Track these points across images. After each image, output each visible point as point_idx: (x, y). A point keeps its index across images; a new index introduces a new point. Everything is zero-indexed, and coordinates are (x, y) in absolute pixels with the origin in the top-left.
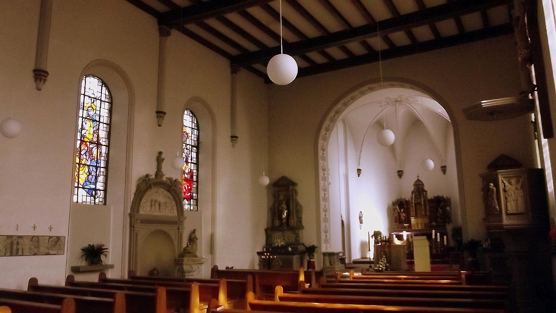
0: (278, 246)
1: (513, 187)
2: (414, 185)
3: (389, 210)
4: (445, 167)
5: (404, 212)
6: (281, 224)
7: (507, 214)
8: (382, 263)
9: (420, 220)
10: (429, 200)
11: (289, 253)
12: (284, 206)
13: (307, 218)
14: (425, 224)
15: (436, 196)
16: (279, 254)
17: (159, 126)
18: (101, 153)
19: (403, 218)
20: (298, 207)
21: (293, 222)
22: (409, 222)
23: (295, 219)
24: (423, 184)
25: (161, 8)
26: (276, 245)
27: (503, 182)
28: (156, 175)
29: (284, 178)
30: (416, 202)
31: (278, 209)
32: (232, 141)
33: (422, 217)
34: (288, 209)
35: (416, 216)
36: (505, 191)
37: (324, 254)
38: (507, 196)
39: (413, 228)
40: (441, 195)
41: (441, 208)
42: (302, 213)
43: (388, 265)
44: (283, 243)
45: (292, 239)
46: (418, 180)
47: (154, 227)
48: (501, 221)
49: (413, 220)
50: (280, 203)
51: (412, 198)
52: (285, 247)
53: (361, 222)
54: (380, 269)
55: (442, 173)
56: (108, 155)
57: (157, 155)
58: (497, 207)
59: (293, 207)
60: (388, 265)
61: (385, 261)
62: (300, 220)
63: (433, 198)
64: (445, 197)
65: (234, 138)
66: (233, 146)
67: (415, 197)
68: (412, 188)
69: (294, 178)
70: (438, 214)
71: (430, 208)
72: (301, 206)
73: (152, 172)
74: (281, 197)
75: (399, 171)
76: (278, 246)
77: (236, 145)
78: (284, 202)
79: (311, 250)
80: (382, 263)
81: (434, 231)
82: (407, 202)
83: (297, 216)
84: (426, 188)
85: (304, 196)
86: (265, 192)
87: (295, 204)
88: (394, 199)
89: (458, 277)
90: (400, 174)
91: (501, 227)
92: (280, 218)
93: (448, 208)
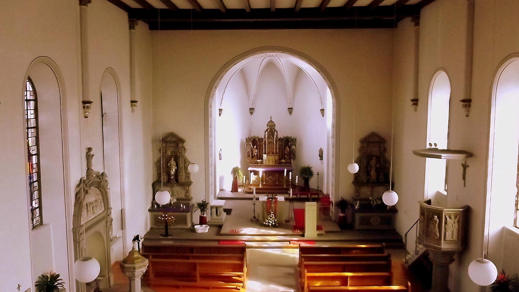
1: (452, 221)
3: (242, 145)
4: (222, 110)
6: (169, 180)
7: (445, 240)
9: (272, 158)
10: (279, 139)
11: (184, 211)
12: (173, 162)
15: (285, 136)
17: (86, 117)
18: (32, 165)
21: (182, 178)
25: (134, 5)
27: (445, 216)
28: (87, 176)
30: (269, 141)
34: (177, 165)
36: (446, 223)
37: (212, 208)
38: (447, 227)
41: (290, 147)
48: (440, 244)
49: (265, 156)
50: (168, 161)
52: (177, 205)
56: (38, 164)
57: (85, 152)
58: (438, 234)
61: (274, 217)
62: (188, 175)
63: (282, 137)
64: (292, 137)
66: (133, 111)
69: (182, 135)
73: (84, 175)
74: (169, 153)
75: (251, 109)
79: (203, 206)
81: (286, 170)
82: (261, 140)
84: (276, 128)
85: (192, 151)
89: (407, 286)
90: (252, 111)
91: (440, 249)
92: (169, 174)
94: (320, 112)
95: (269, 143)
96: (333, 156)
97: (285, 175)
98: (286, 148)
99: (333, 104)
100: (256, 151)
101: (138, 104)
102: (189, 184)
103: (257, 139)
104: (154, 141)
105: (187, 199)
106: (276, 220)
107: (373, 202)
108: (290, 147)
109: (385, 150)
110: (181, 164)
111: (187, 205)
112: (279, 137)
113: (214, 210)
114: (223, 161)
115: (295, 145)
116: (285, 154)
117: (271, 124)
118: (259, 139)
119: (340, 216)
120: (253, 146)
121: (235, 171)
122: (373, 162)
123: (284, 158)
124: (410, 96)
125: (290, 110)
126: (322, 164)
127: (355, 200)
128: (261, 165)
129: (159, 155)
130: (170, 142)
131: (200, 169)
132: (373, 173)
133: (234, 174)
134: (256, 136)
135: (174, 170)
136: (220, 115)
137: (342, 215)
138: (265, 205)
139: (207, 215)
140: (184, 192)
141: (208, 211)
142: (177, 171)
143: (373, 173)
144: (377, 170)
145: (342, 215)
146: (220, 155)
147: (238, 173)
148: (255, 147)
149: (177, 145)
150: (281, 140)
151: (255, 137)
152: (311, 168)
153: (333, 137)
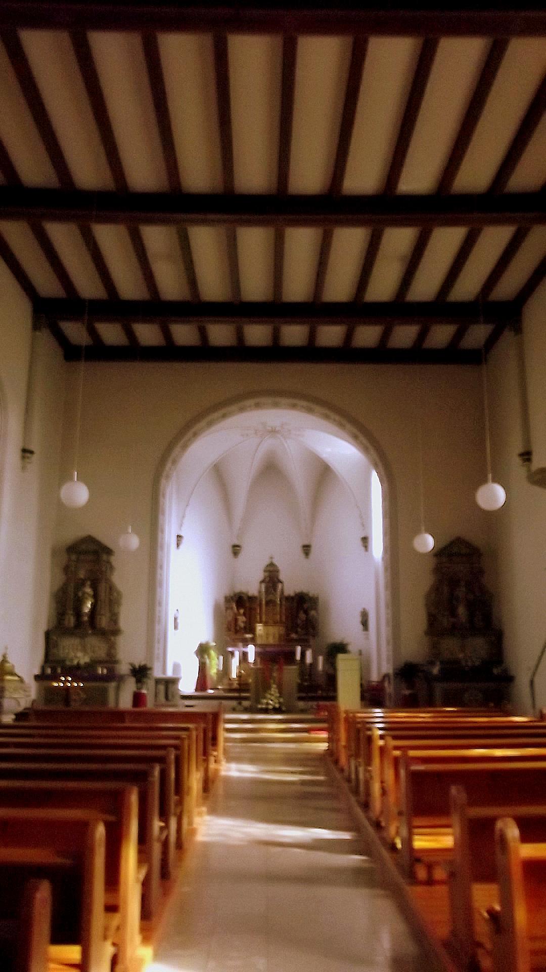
0: (78, 664)
2: (265, 571)
5: (244, 614)
6: (79, 624)
8: (273, 698)
12: (88, 590)
13: (129, 617)
14: (280, 636)
15: (298, 591)
20: (115, 594)
21: (103, 621)
22: (252, 630)
23: (108, 615)
24: (278, 571)
26: (75, 662)
29: (90, 539)
31: (76, 595)
32: (23, 458)
33: (275, 623)
34: (95, 596)
35: (266, 624)
37: (158, 681)
40: (305, 591)
43: (281, 700)
45: (101, 653)
46: (272, 564)
49: (259, 628)
51: (260, 592)
53: (176, 627)
54: (271, 707)
60: (281, 700)
61: (278, 695)
62: (114, 619)
64: (311, 595)
65: (26, 452)
66: (24, 468)
68: (260, 575)
69: (105, 539)
70: (299, 622)
72: (119, 593)
74: (82, 574)
76: (78, 664)
77: (29, 466)
79: (141, 673)
80: (273, 698)
82: (251, 599)
83: (110, 611)
84: (282, 577)
85: (124, 577)
88: (226, 592)
90: (236, 550)
92: (78, 613)
93: (313, 613)
94: (359, 543)
95: (267, 603)
96: (387, 623)
97: (298, 657)
98: (299, 615)
99: (384, 507)
100: (244, 619)
101: (35, 458)
102: (116, 632)
103: (245, 598)
104: (55, 553)
105: (111, 660)
107: (466, 661)
109: (481, 572)
110: (103, 595)
113: (162, 688)
114: (182, 628)
115: (316, 609)
116: (298, 625)
117: (271, 569)
119: (405, 696)
120: (238, 609)
121: (202, 651)
122: (461, 592)
123: (296, 633)
124: (516, 446)
125: (307, 549)
126: (367, 638)
128: (253, 641)
129: (61, 578)
130: (86, 553)
131: (141, 542)
132: (461, 610)
135: (89, 606)
136: (178, 545)
137: (407, 692)
141: (151, 683)
142: (94, 606)
143: (461, 610)
144: (470, 606)
146: (176, 619)
147: (209, 655)
150: (289, 599)
151: (241, 593)
153: (386, 569)
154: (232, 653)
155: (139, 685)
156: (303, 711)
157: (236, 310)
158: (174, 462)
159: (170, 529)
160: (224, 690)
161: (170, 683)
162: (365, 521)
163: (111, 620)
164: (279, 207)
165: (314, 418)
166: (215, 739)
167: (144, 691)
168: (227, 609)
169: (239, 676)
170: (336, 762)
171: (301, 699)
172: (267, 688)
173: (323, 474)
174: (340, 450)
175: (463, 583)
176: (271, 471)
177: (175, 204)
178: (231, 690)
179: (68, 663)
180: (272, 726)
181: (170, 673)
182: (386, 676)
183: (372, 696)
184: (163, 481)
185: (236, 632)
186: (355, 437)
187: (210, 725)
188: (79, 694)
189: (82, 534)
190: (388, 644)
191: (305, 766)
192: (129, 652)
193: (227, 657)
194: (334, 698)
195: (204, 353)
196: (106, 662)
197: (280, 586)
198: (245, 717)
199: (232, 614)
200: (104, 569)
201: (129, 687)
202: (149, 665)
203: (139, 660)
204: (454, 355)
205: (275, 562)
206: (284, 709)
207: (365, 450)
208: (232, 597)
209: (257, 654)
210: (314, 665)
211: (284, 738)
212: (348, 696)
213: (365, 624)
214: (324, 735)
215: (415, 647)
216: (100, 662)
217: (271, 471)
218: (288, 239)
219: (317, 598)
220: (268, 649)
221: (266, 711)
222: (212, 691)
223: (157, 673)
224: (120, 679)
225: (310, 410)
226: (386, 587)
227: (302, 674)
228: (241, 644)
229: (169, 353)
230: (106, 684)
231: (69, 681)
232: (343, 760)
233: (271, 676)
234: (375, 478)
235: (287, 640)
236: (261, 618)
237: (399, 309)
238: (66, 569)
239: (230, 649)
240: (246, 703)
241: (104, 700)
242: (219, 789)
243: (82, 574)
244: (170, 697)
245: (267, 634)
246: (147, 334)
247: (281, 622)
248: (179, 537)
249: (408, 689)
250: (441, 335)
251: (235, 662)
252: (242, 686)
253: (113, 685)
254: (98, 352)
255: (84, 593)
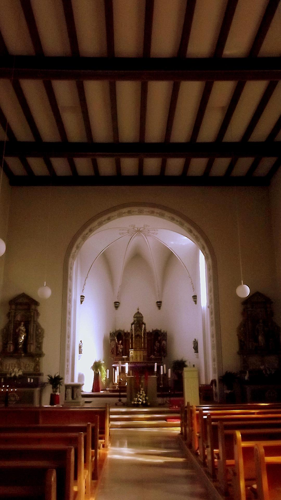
0: (15, 376)
2: (134, 317)
3: (105, 341)
4: (160, 302)
5: (122, 344)
8: (141, 397)
10: (148, 333)
12: (22, 328)
13: (49, 345)
15: (154, 329)
16: (17, 386)
19: (121, 350)
20: (40, 330)
21: (32, 349)
22: (128, 354)
23: (35, 343)
24: (142, 317)
26: (13, 375)
29: (24, 296)
30: (136, 334)
33: (141, 349)
34: (27, 332)
35: (135, 349)
37: (67, 387)
39: (130, 361)
42: (43, 337)
44: (21, 373)
47: (115, 348)
49: (132, 352)
50: (17, 325)
51: (131, 330)
52: (24, 377)
53: (80, 352)
55: (157, 308)
59: (33, 330)
61: (144, 395)
62: (39, 346)
63: (151, 331)
64: (162, 331)
67: (135, 330)
70: (155, 348)
71: (148, 341)
72: (43, 330)
74: (19, 318)
75: (115, 303)
78: (23, 323)
79: (56, 381)
81: (156, 364)
82: (127, 334)
83: (36, 341)
84: (145, 320)
85: (46, 319)
86: (240, 308)
87: (35, 326)
88: (111, 330)
90: (117, 305)
92: (16, 343)
97: (156, 370)
100: (122, 347)
102: (40, 355)
103: (123, 334)
105: (37, 374)
106: (147, 398)
108: (160, 342)
111: (36, 380)
112: (147, 331)
113: (70, 391)
114: (84, 351)
115: (166, 340)
117: (138, 316)
118: (125, 334)
119: (226, 393)
120: (118, 341)
121: (96, 366)
125: (159, 304)
126: (198, 357)
127: (243, 372)
128: (128, 360)
130: (21, 304)
133: (96, 370)
134: (122, 329)
136: (81, 302)
137: (228, 392)
138: (133, 382)
139: (60, 393)
140: (32, 365)
141: (63, 388)
142: (26, 338)
145: (228, 392)
146: (80, 347)
148: (120, 342)
149: (29, 309)
150: (149, 334)
152: (185, 361)
153: (211, 313)
154: (115, 368)
155: (55, 390)
156: (161, 405)
157: (116, 148)
158: (78, 247)
159: (75, 293)
160: (109, 390)
161: (76, 388)
162: (195, 285)
163: (37, 347)
164: (144, 67)
165: (165, 220)
166: (103, 431)
167: (58, 393)
168: (111, 340)
169: (120, 382)
170: (190, 446)
171: (159, 396)
172: (137, 390)
173: (169, 257)
174: (181, 241)
175: (261, 321)
176: (137, 257)
177: (76, 66)
178: (113, 391)
179: (8, 376)
180: (142, 416)
181: (76, 381)
182: (213, 382)
183: (206, 394)
184: (71, 259)
185: (117, 354)
186: (190, 231)
187: (99, 417)
188: (14, 396)
189: (22, 292)
190: (214, 360)
191: (166, 448)
192: (48, 368)
193: (112, 371)
194: (182, 395)
195: (96, 180)
196: (35, 375)
197: (143, 326)
198: (124, 410)
199: (114, 343)
200: (32, 314)
201: (49, 390)
202: (61, 377)
203: (54, 373)
204: (250, 180)
205: (140, 311)
206: (149, 404)
207: (196, 239)
208: (114, 333)
209: (130, 368)
210: (166, 375)
211: (150, 425)
212: (191, 396)
213: (196, 349)
214: (179, 422)
215: (232, 362)
216: (30, 375)
217: (137, 257)
218: (149, 87)
219: (166, 333)
220: (138, 365)
221: (137, 406)
222: (102, 392)
223: (67, 381)
224: (43, 385)
225: (162, 215)
226: (212, 324)
227: (158, 379)
228: (120, 362)
229: (75, 180)
230: (32, 389)
231: (7, 388)
232: (196, 444)
233: (140, 383)
234: (202, 257)
235: (148, 359)
236: (132, 345)
237: (218, 147)
238: (9, 315)
239: (113, 365)
240: (124, 400)
241: (31, 398)
242: (106, 472)
243: (19, 318)
244: (75, 397)
245: (136, 356)
246: (60, 166)
247: (144, 348)
248: (82, 296)
249: (228, 389)
250: (244, 164)
251: (117, 373)
252: (122, 388)
253: (38, 389)
254: (29, 180)
255: (20, 330)
